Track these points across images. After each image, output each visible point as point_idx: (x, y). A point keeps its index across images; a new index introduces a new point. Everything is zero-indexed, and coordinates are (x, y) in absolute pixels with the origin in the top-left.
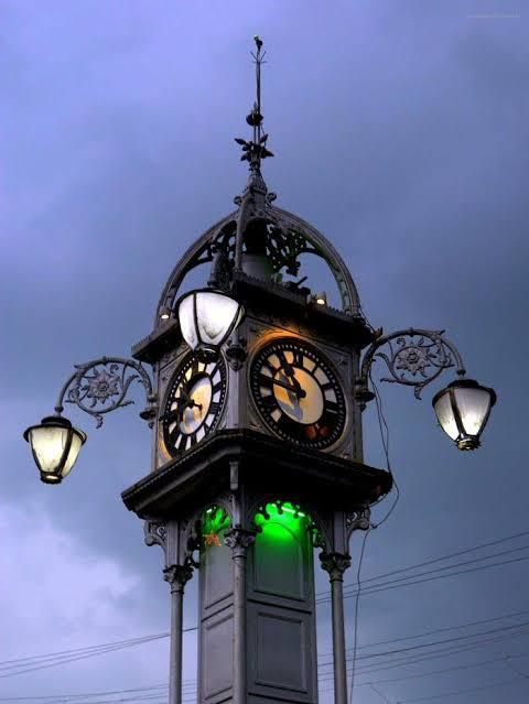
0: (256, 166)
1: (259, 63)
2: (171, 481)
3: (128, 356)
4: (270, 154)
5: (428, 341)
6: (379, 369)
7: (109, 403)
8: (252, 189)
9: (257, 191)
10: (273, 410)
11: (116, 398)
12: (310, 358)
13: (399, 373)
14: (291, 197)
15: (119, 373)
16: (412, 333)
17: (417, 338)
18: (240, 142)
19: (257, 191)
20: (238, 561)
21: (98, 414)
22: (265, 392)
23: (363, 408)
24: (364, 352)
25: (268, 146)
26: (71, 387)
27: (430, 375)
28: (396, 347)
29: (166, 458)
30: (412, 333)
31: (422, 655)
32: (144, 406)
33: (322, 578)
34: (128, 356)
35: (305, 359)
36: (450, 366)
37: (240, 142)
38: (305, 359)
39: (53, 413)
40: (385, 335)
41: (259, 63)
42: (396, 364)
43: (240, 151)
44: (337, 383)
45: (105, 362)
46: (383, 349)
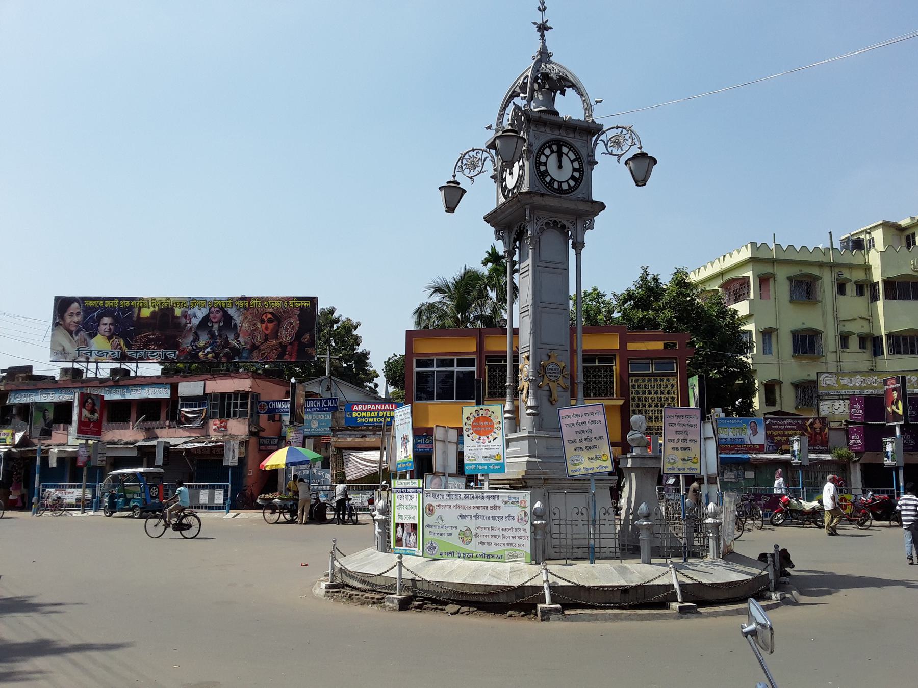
0: (542, 36)
2: (730, 611)
3: (484, 148)
4: (551, 28)
5: (625, 132)
6: (600, 148)
7: (476, 172)
8: (540, 53)
9: (544, 55)
11: (479, 169)
14: (564, 60)
15: (479, 156)
18: (535, 24)
19: (544, 55)
21: (471, 178)
22: (542, 168)
24: (594, 139)
25: (548, 24)
26: (459, 164)
29: (502, 200)
31: (488, 517)
32: (492, 173)
33: (572, 252)
34: (484, 148)
37: (535, 24)
39: (451, 179)
43: (535, 28)
45: (473, 150)
46: (603, 137)
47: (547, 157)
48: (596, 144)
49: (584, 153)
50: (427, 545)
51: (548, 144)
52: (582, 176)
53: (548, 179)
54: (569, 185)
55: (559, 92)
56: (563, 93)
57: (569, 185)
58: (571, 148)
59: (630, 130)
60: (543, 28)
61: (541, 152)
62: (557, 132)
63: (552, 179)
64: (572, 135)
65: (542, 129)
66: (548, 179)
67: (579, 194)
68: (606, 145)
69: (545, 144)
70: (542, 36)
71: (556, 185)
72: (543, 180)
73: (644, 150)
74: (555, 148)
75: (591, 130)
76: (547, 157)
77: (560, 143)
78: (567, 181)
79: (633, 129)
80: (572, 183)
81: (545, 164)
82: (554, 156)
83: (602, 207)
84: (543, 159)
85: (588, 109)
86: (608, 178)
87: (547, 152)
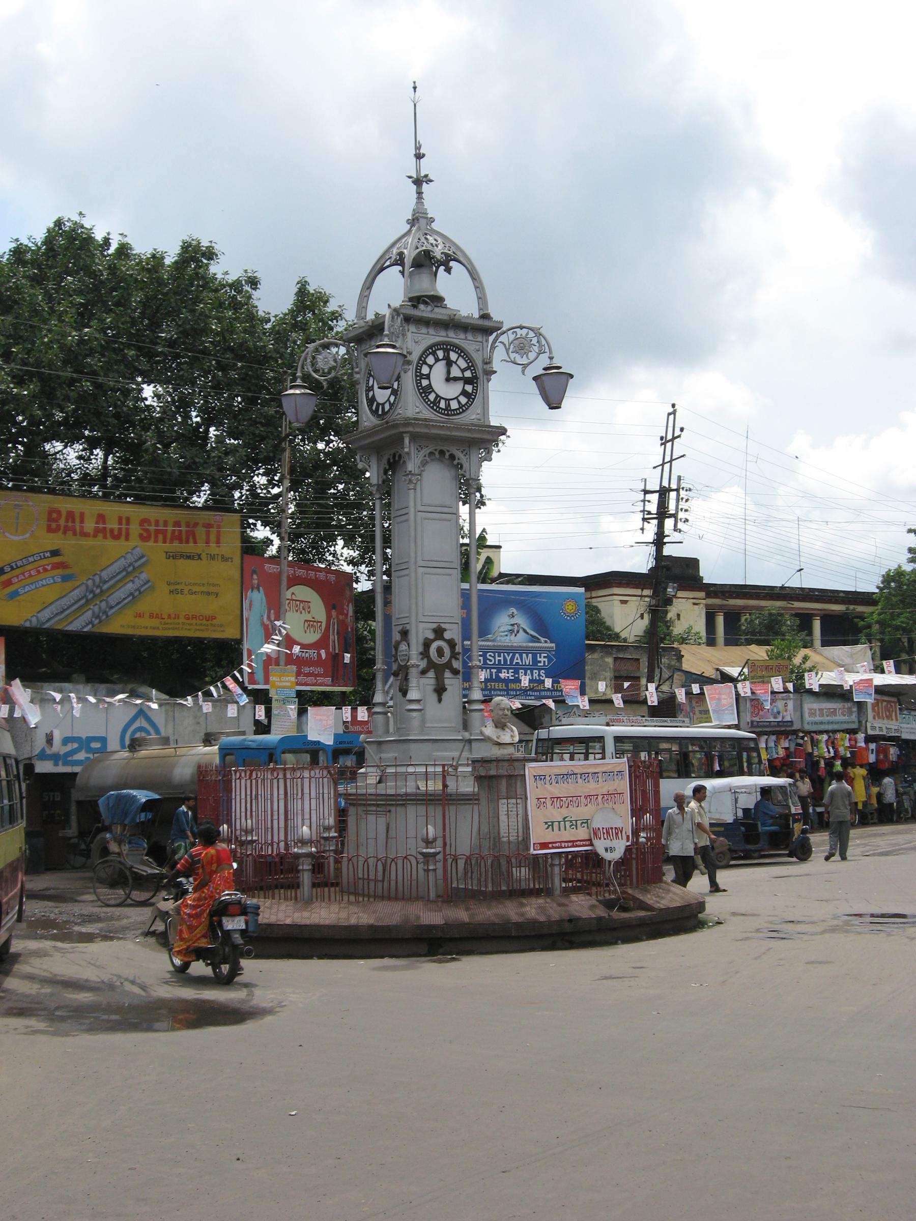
0: (420, 193)
1: (827, 901)
6: (499, 354)
10: (430, 393)
12: (455, 351)
13: (512, 355)
14: (451, 223)
16: (521, 328)
17: (525, 331)
18: (410, 177)
19: (419, 218)
20: (723, 877)
22: (425, 383)
23: (489, 380)
27: (532, 359)
28: (512, 337)
30: (521, 328)
35: (451, 353)
36: (544, 352)
37: (410, 177)
38: (451, 353)
40: (504, 329)
41: (827, 901)
42: (511, 350)
44: (472, 366)
46: (503, 338)
47: (431, 367)
48: (493, 347)
49: (478, 359)
50: (69, 585)
51: (431, 350)
52: (475, 389)
53: (432, 397)
54: (459, 402)
55: (442, 268)
56: (448, 270)
57: (459, 402)
58: (462, 352)
59: (538, 333)
60: (419, 182)
61: (422, 361)
62: (443, 333)
63: (437, 396)
64: (462, 336)
65: (424, 330)
66: (432, 397)
67: (471, 416)
68: (507, 350)
69: (427, 349)
70: (420, 193)
71: (442, 404)
72: (426, 400)
73: (556, 363)
74: (440, 354)
75: (484, 327)
76: (431, 367)
77: (448, 347)
78: (456, 398)
79: (542, 331)
80: (463, 400)
81: (428, 377)
82: (441, 365)
83: (495, 372)
84: (425, 370)
85: (482, 299)
86: (507, 398)
87: (430, 360)
